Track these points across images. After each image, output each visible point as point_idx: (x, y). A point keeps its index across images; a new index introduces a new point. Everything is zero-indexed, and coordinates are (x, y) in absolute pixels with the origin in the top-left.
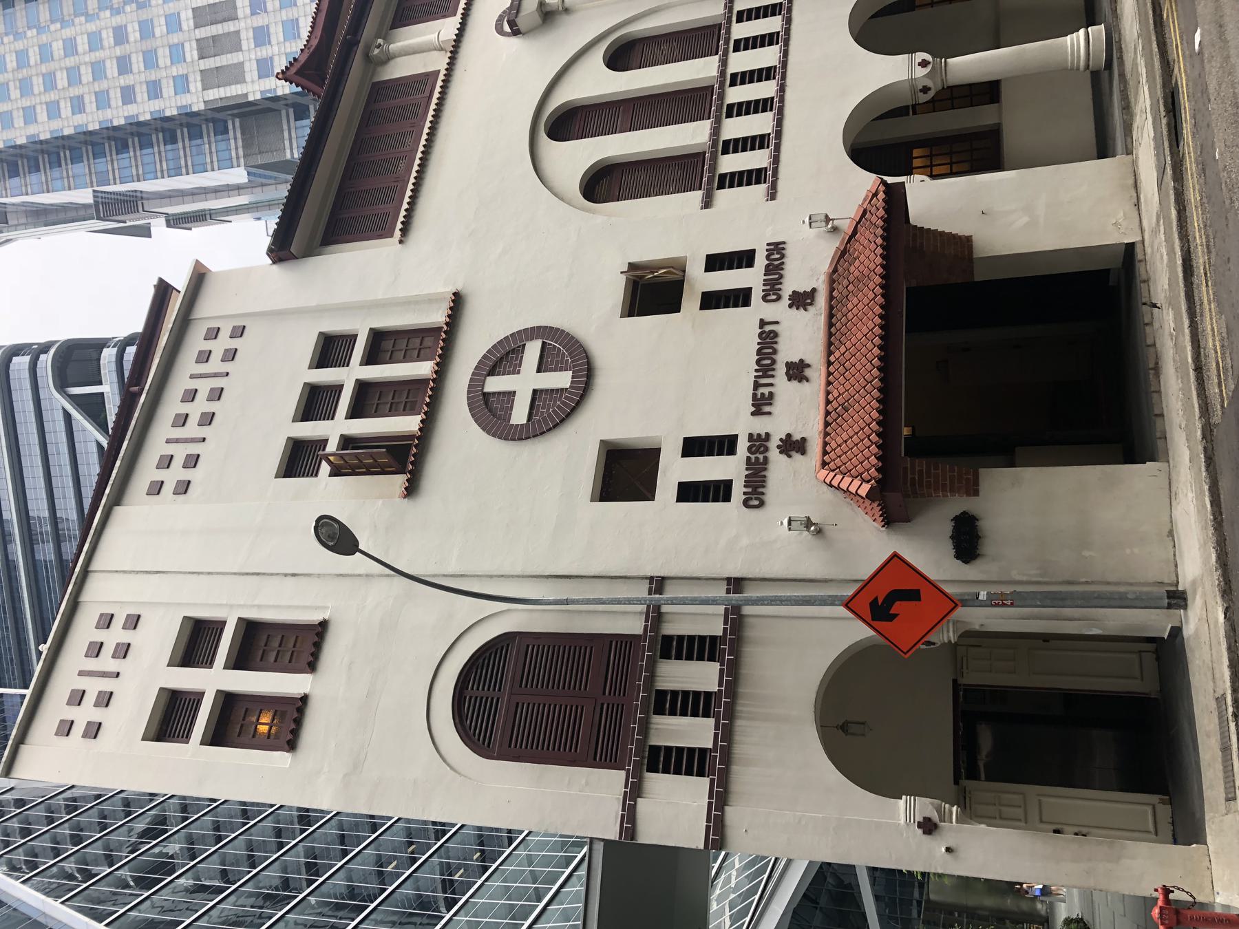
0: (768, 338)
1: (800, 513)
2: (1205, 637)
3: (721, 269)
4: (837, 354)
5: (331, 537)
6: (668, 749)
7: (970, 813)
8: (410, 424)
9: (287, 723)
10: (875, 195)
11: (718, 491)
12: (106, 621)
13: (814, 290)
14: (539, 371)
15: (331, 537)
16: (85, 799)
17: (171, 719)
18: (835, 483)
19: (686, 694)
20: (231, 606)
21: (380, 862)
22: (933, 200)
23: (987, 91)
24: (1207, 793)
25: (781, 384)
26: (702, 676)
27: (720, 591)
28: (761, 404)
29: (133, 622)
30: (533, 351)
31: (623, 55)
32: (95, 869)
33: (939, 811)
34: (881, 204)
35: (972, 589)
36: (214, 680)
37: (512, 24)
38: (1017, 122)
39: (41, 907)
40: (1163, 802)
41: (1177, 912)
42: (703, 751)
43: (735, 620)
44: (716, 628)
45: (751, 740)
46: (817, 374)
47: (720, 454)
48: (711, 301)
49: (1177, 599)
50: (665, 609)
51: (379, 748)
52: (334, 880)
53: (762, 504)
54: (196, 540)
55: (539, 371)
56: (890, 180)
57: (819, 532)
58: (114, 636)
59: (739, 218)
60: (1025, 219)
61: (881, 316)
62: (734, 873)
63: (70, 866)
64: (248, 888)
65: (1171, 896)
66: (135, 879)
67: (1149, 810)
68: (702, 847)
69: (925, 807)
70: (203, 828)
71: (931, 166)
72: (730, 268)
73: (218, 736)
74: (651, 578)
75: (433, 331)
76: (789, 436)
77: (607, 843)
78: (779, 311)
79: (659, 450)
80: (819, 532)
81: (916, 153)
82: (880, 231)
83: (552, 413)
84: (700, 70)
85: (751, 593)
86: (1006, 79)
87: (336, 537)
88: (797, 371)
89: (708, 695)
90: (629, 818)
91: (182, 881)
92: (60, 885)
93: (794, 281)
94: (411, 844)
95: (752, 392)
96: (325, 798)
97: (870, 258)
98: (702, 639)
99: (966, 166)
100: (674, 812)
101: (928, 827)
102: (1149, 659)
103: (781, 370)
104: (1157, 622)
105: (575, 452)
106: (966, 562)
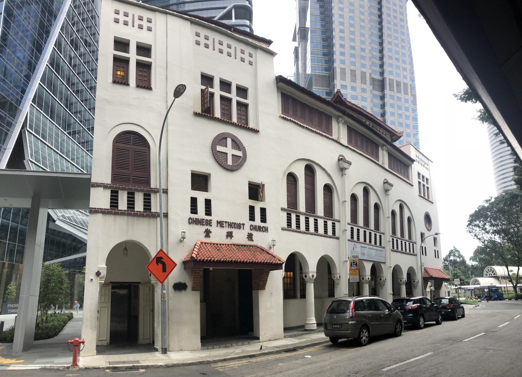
0: (239, 226)
1: (187, 235)
2: (155, 358)
3: (261, 212)
4: (234, 247)
5: (179, 89)
6: (118, 196)
7: (103, 286)
8: (218, 113)
9: (121, 81)
10: (280, 260)
11: (194, 210)
12: (149, 21)
13: (253, 241)
14: (232, 155)
15: (179, 89)
16: (95, 21)
17: (121, 44)
18: (196, 246)
19: (134, 201)
20: (156, 59)
21: (80, 112)
22: (276, 279)
23: (303, 296)
24: (111, 356)
25: (227, 229)
26: (139, 206)
27: (164, 211)
28: (220, 224)
29: (149, 29)
30: (239, 153)
31: (377, 207)
32: (75, 26)
33: (103, 277)
34: (277, 262)
35: (166, 288)
36: (133, 56)
37: (341, 159)
38: (294, 303)
39: (64, 11)
40: (107, 343)
41: (77, 346)
42: (117, 207)
43: (155, 216)
44: (153, 210)
45: (121, 221)
46: (229, 241)
47: (206, 211)
48: (252, 209)
49: (165, 351)
50: (158, 194)
51: (116, 109)
52: (75, 98)
53: (190, 223)
54: (178, 47)
55: (232, 155)
56: (284, 265)
57: (181, 241)
58: (145, 24)
59: (277, 218)
60: (269, 306)
61: (243, 261)
62: (81, 217)
63: (76, 19)
64: (71, 73)
65: (82, 344)
66: (73, 39)
67: (105, 339)
68: (90, 207)
69: (104, 273)
70: (88, 58)
71: (287, 278)
72: (261, 215)
73: (116, 59)
74: (167, 189)
75: (247, 123)
76: (211, 232)
77: (90, 179)
78: (247, 230)
79: (207, 191)
80: (181, 241)
81: (292, 273)
82: (268, 261)
83: (219, 159)
84: (320, 210)
85: (164, 220)
86: (306, 301)
87: (179, 91)
88: (230, 235)
89: (134, 208)
90: (98, 185)
91: (73, 53)
92: (70, 16)
93: (256, 235)
94: (86, 121)
95: (224, 221)
96: (99, 93)
97: (261, 258)
98: (150, 206)
99: (286, 287)
100: (100, 198)
101: (98, 274)
102: (147, 341)
103: (230, 230)
104: (158, 345)
105: (207, 165)
106: (173, 287)
